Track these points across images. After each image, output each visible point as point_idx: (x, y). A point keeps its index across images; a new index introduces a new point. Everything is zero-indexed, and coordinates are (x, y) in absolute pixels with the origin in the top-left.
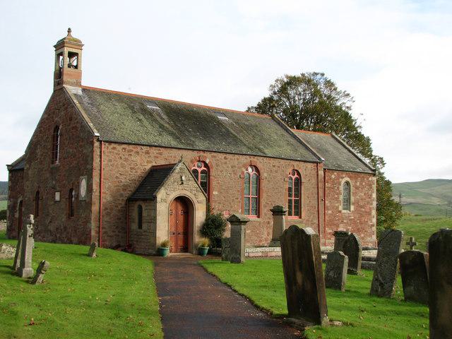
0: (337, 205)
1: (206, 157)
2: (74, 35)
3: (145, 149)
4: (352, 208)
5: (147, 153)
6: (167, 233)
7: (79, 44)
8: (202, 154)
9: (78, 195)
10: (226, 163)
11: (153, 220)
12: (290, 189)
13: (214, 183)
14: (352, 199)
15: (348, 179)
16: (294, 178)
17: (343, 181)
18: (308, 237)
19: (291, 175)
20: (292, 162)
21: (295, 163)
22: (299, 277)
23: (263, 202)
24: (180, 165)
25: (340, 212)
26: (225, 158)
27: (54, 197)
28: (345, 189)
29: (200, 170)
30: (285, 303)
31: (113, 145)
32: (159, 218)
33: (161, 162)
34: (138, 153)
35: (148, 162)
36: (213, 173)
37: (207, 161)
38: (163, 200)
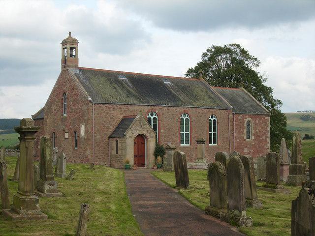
1: (156, 109)
2: (74, 36)
5: (120, 108)
7: (76, 42)
15: (250, 119)
17: (246, 120)
25: (245, 140)
34: (114, 109)
38: (130, 137)
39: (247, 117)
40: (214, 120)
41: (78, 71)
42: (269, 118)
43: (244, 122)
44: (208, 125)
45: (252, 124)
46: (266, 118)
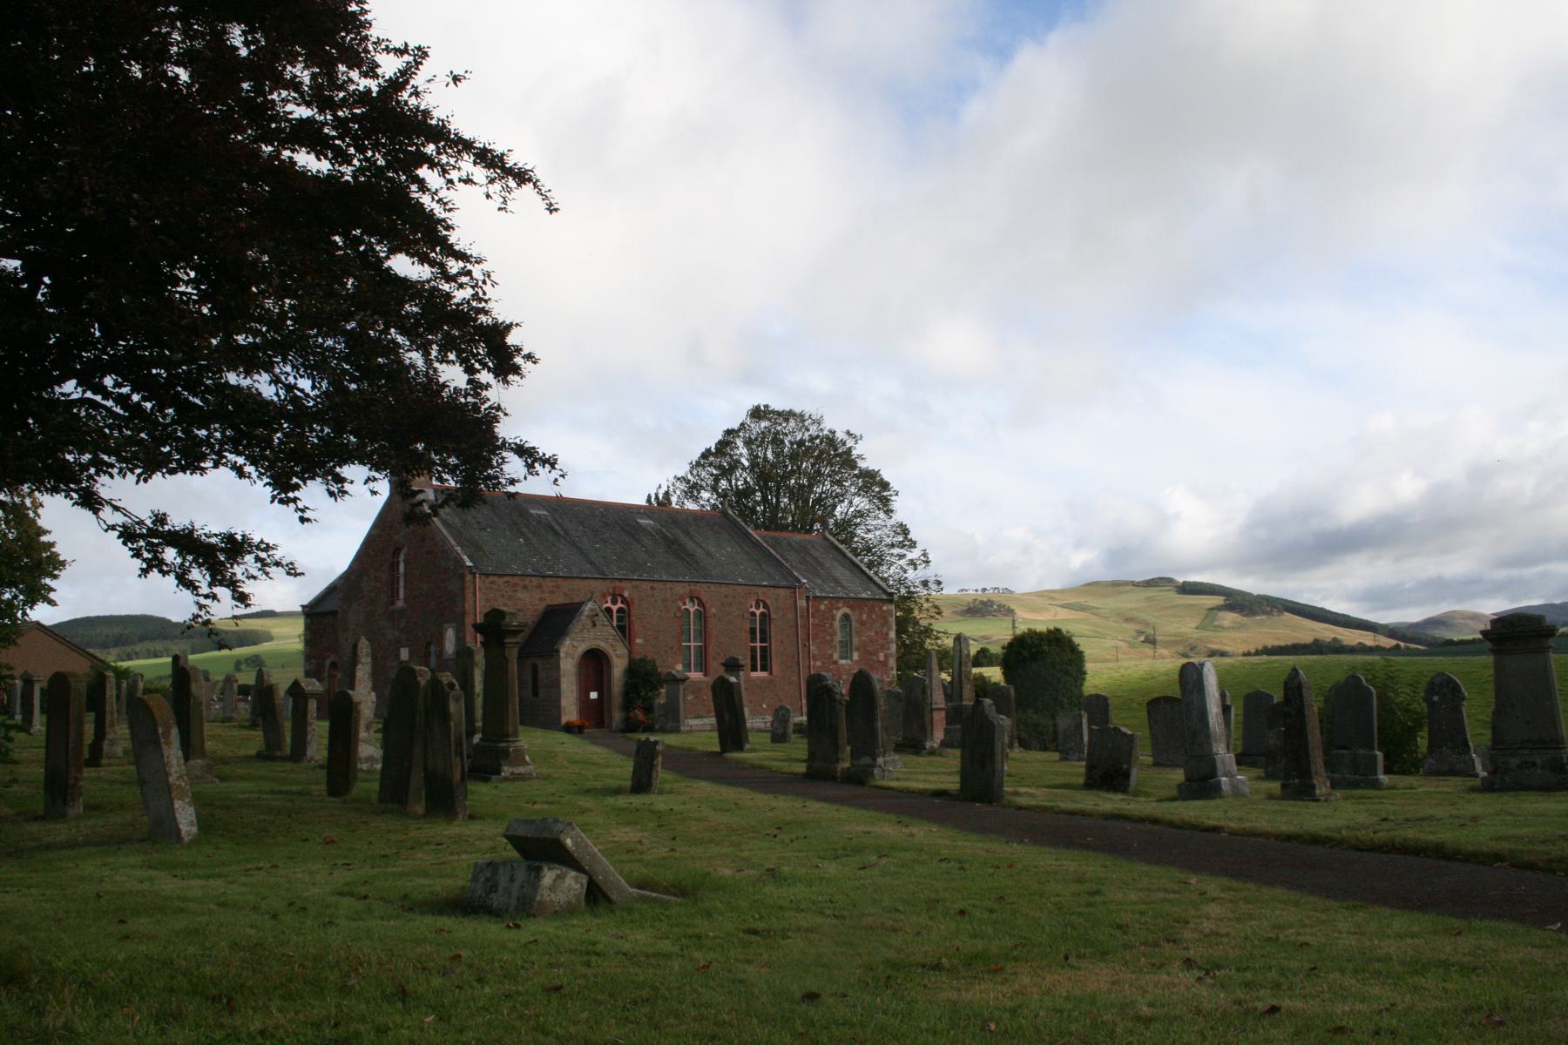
3: (535, 581)
4: (856, 656)
5: (539, 586)
9: (441, 652)
11: (556, 684)
12: (753, 631)
13: (637, 627)
14: (856, 641)
15: (847, 610)
16: (615, 608)
17: (839, 614)
18: (732, 684)
21: (760, 590)
22: (727, 717)
23: (712, 650)
24: (590, 605)
27: (398, 656)
28: (843, 627)
29: (615, 608)
30: (717, 741)
31: (492, 578)
32: (563, 680)
33: (559, 599)
34: (525, 587)
36: (634, 612)
37: (626, 594)
43: (833, 617)
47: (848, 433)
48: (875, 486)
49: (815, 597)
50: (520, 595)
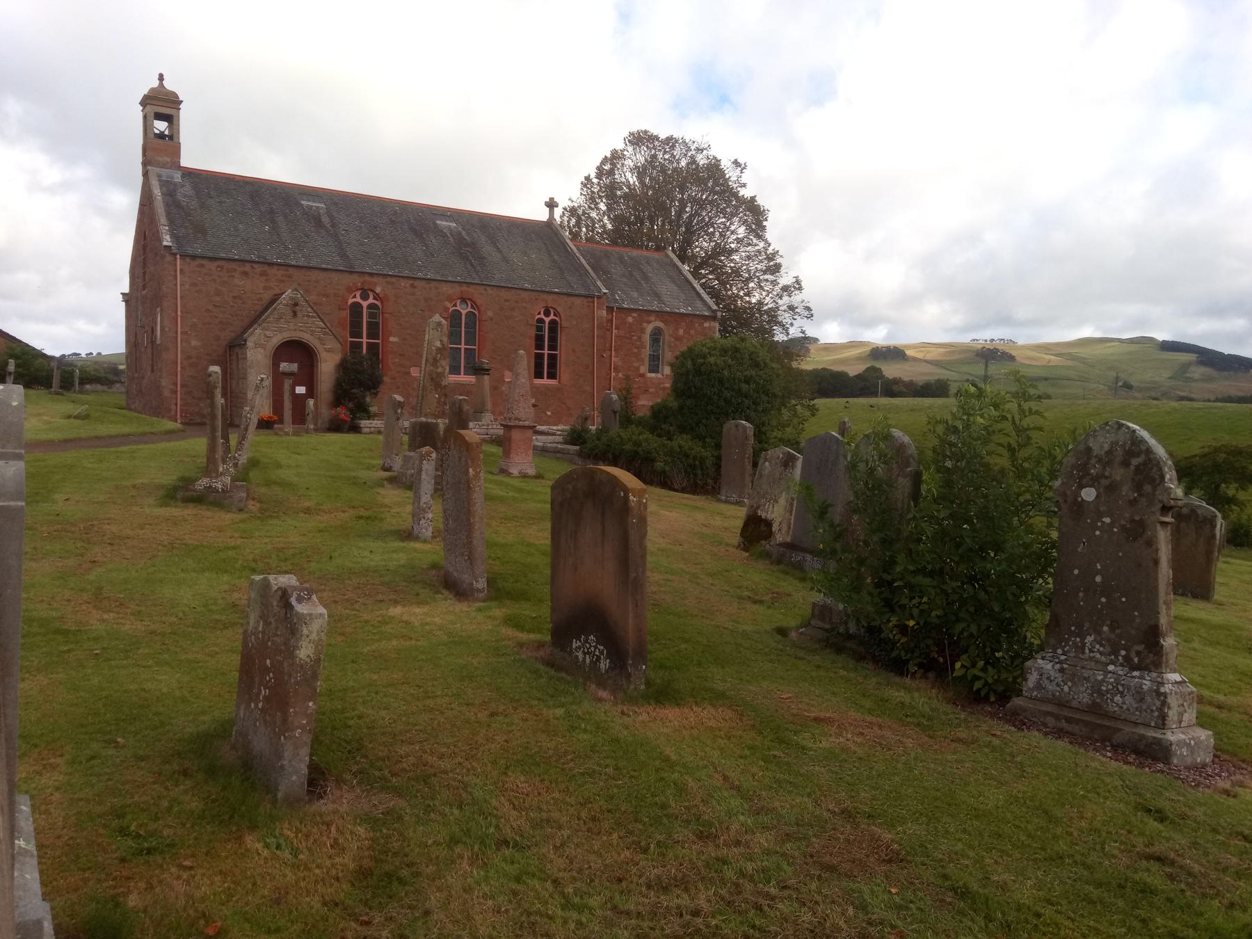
0: (636, 365)
1: (375, 284)
2: (169, 85)
3: (258, 268)
5: (263, 274)
6: (878, 336)
7: (174, 101)
8: (368, 278)
10: (413, 294)
15: (660, 324)
16: (547, 320)
17: (649, 328)
19: (542, 316)
20: (545, 296)
21: (550, 298)
25: (642, 375)
26: (413, 286)
31: (199, 261)
34: (245, 273)
35: (265, 288)
37: (378, 290)
38: (257, 345)
39: (652, 318)
40: (553, 323)
41: (177, 177)
42: (717, 325)
43: (643, 331)
44: (533, 332)
45: (667, 337)
46: (706, 325)
47: (736, 163)
48: (755, 215)
49: (620, 309)
50: (237, 281)
